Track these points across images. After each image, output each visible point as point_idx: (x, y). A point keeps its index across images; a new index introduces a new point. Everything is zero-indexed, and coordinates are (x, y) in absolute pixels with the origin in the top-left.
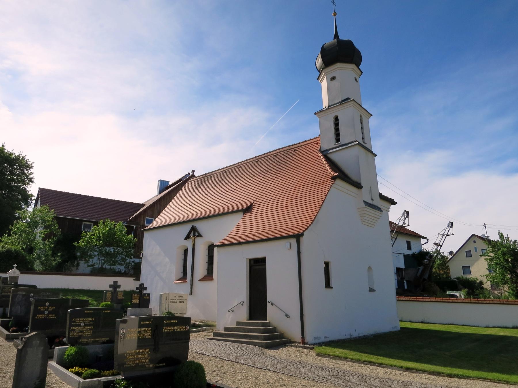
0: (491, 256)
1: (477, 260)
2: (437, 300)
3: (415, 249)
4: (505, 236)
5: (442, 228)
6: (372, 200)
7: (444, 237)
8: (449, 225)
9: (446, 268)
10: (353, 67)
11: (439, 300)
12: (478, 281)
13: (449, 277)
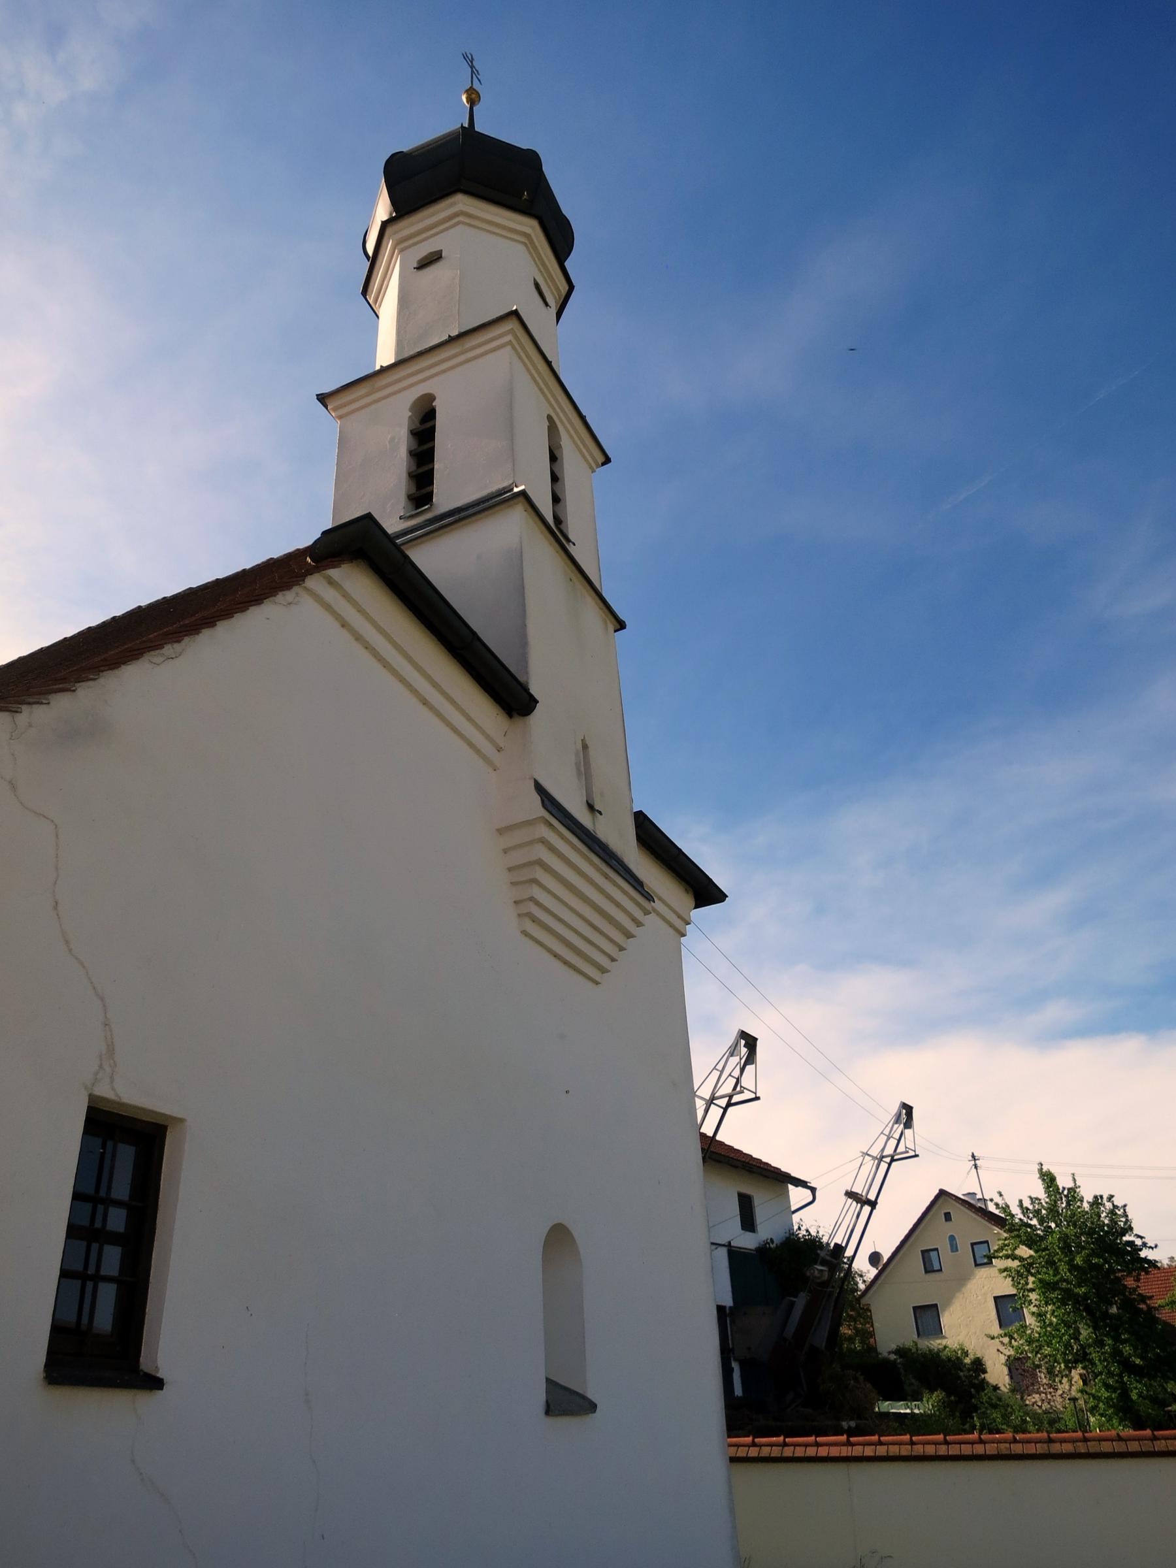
0: (1021, 1259)
1: (962, 1280)
2: (919, 1450)
3: (767, 1230)
4: (1064, 1182)
5: (874, 1132)
6: (591, 807)
7: (884, 1166)
8: (899, 1116)
9: (859, 1315)
10: (528, 230)
11: (930, 1450)
12: (967, 1361)
13: (873, 1349)
